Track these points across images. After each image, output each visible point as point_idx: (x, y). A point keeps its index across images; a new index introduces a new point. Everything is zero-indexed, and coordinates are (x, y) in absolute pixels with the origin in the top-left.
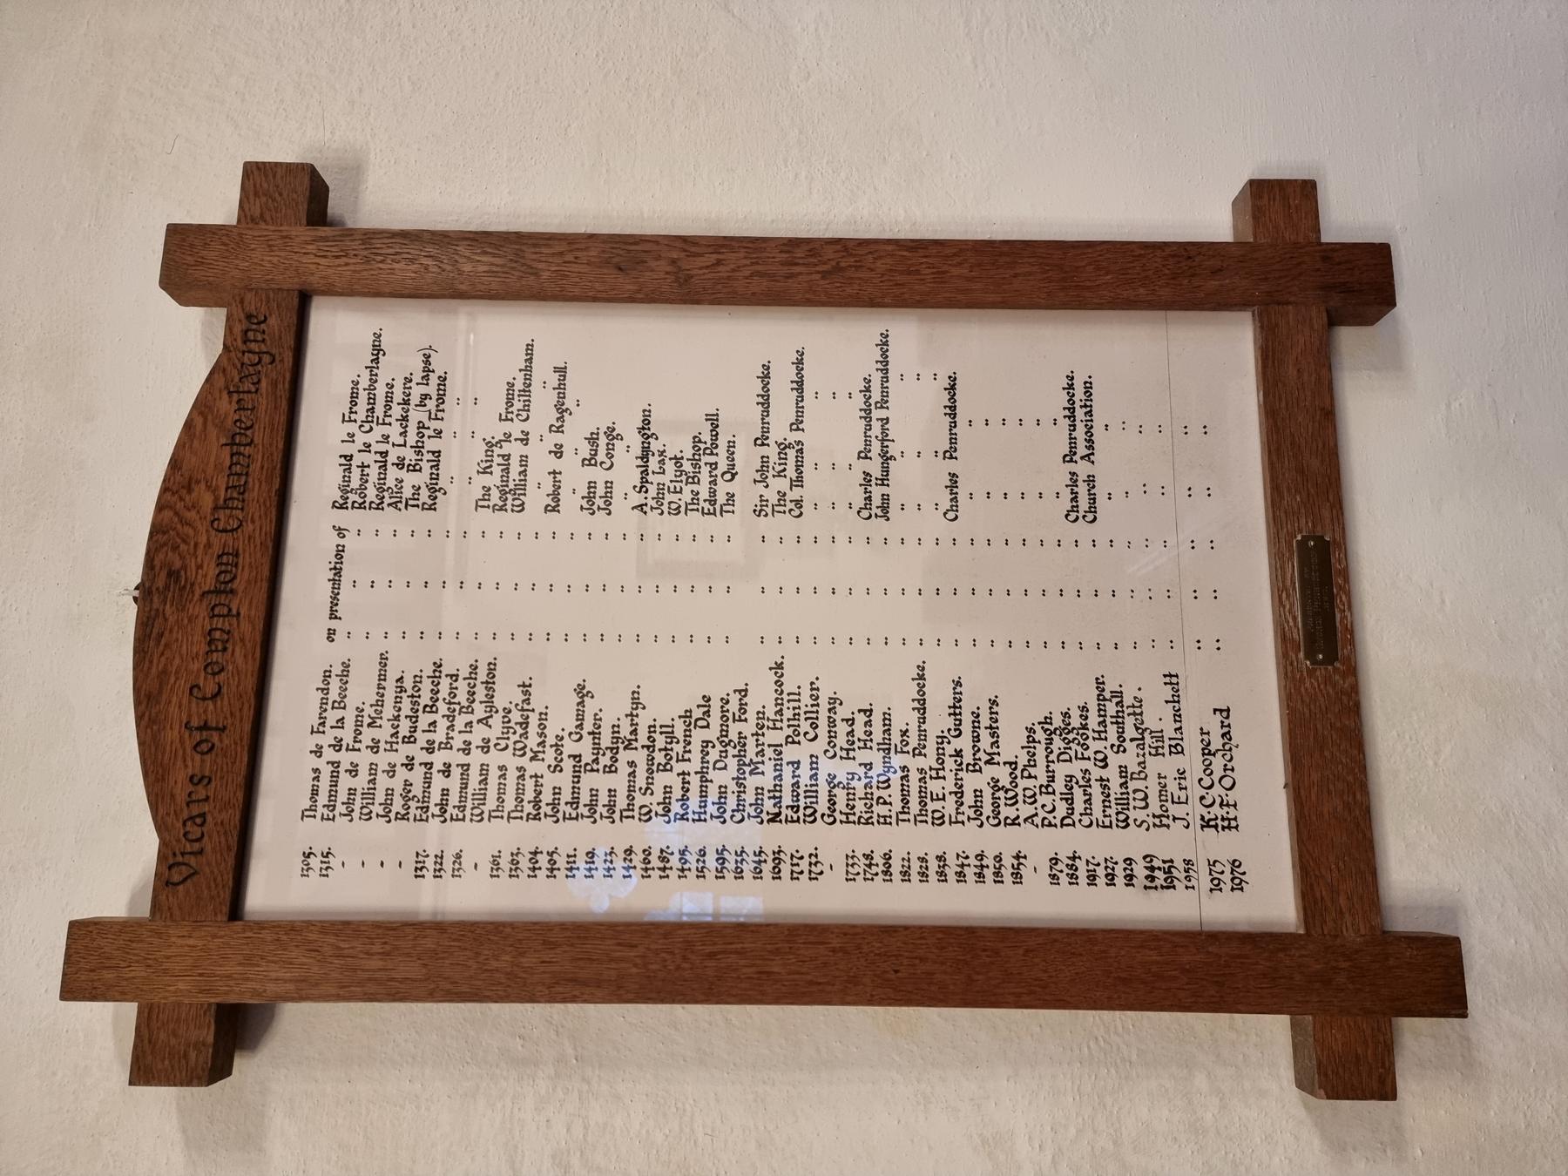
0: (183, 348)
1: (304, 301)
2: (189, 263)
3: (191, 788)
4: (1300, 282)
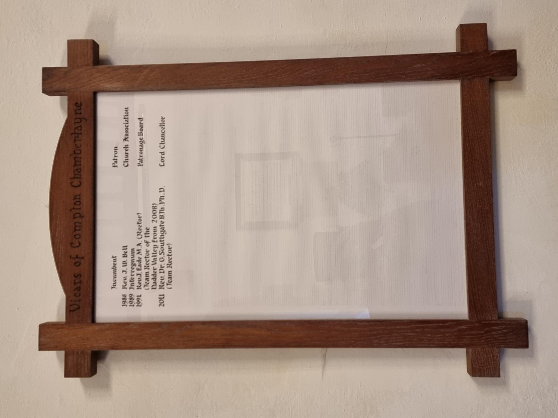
0: (54, 114)
1: (95, 94)
2: (52, 81)
3: (75, 279)
4: (480, 65)
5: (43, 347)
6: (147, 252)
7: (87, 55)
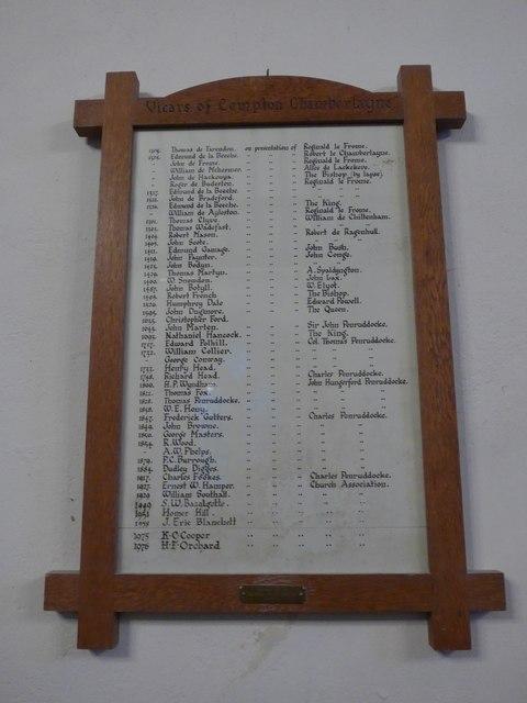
0: (380, 79)
1: (399, 122)
2: (415, 77)
4: (444, 600)
5: (111, 77)
6: (182, 164)
7: (449, 116)
